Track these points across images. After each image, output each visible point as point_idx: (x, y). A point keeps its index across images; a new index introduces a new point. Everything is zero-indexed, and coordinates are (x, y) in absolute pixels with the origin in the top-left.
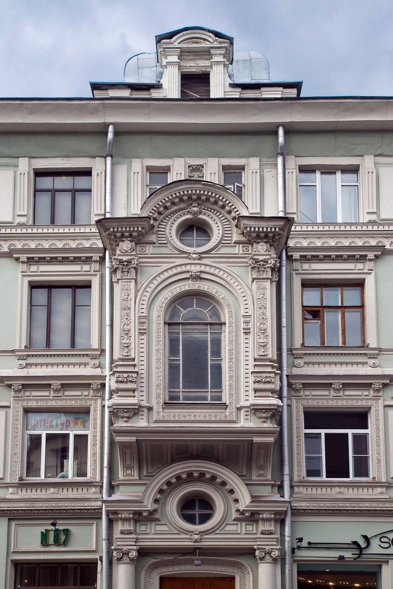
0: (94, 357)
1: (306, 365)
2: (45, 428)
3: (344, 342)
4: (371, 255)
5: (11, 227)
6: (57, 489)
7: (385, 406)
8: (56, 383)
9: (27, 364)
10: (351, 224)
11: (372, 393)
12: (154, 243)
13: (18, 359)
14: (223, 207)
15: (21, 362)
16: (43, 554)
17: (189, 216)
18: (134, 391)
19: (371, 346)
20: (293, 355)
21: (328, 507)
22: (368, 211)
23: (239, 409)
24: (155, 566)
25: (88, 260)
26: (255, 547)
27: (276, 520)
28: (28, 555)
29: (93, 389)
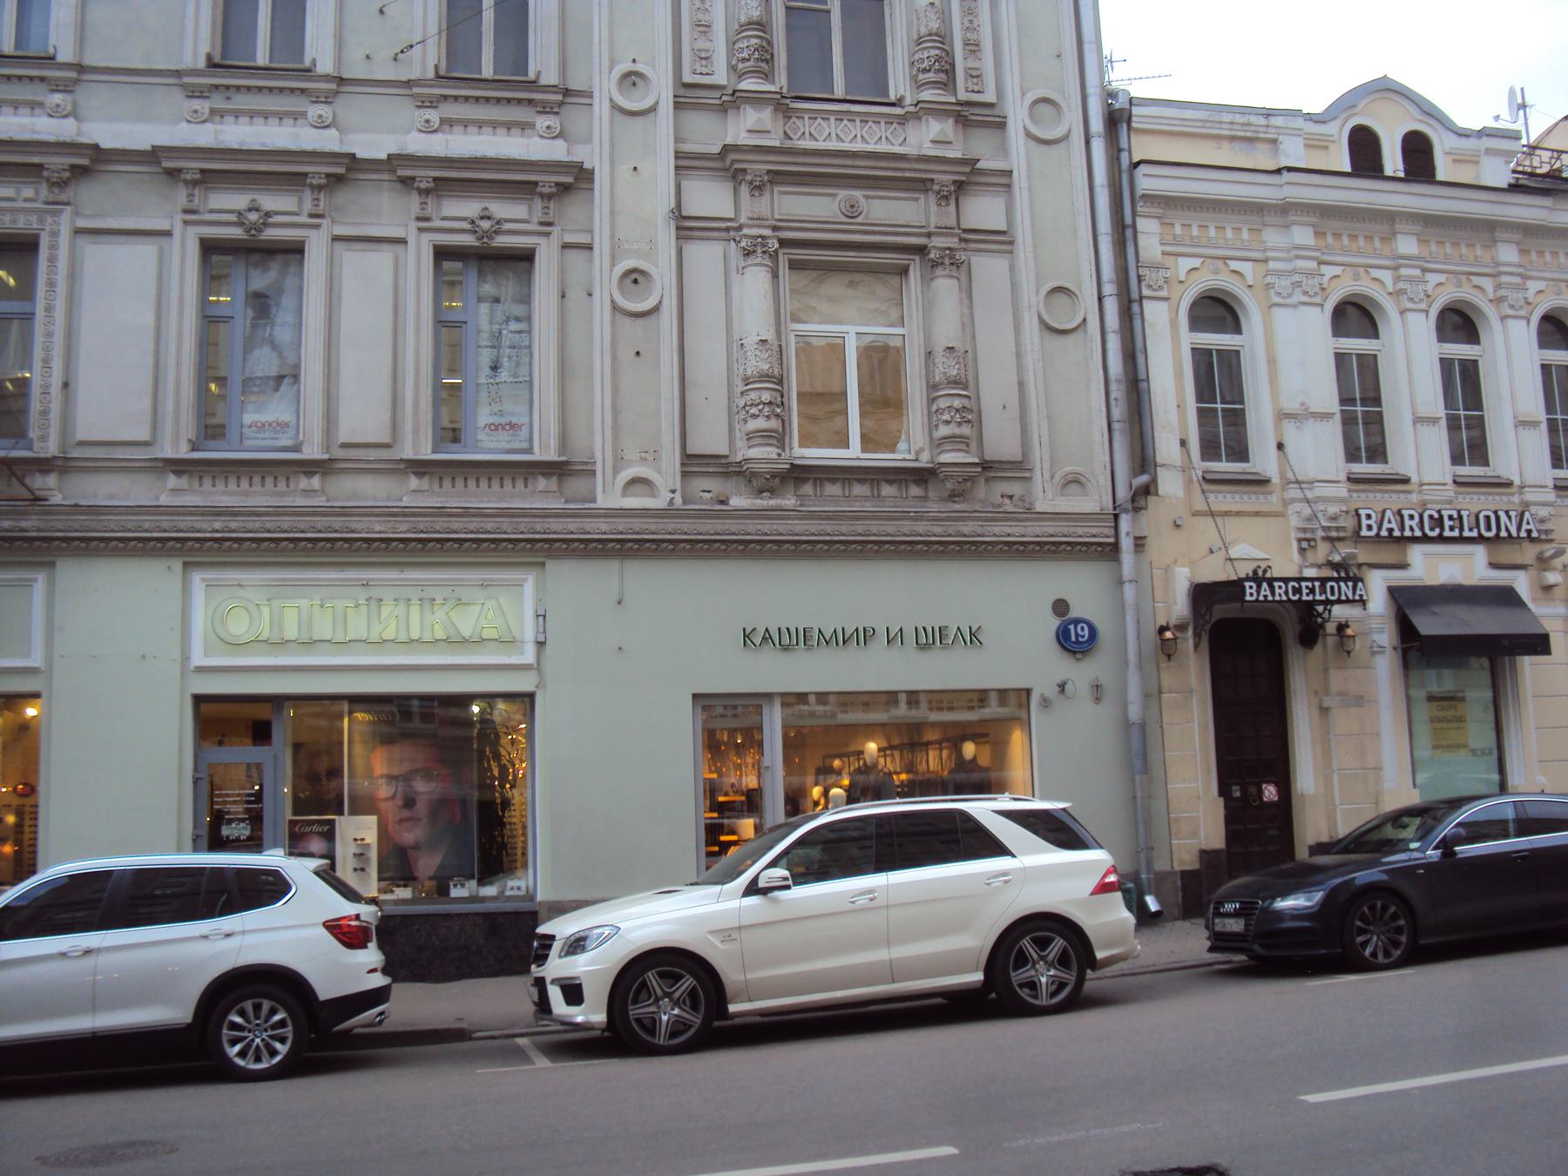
1: (218, 118)
3: (20, 41)
7: (79, 232)
8: (547, 180)
11: (44, 192)
13: (188, 97)
15: (197, 104)
19: (60, 58)
29: (48, 180)
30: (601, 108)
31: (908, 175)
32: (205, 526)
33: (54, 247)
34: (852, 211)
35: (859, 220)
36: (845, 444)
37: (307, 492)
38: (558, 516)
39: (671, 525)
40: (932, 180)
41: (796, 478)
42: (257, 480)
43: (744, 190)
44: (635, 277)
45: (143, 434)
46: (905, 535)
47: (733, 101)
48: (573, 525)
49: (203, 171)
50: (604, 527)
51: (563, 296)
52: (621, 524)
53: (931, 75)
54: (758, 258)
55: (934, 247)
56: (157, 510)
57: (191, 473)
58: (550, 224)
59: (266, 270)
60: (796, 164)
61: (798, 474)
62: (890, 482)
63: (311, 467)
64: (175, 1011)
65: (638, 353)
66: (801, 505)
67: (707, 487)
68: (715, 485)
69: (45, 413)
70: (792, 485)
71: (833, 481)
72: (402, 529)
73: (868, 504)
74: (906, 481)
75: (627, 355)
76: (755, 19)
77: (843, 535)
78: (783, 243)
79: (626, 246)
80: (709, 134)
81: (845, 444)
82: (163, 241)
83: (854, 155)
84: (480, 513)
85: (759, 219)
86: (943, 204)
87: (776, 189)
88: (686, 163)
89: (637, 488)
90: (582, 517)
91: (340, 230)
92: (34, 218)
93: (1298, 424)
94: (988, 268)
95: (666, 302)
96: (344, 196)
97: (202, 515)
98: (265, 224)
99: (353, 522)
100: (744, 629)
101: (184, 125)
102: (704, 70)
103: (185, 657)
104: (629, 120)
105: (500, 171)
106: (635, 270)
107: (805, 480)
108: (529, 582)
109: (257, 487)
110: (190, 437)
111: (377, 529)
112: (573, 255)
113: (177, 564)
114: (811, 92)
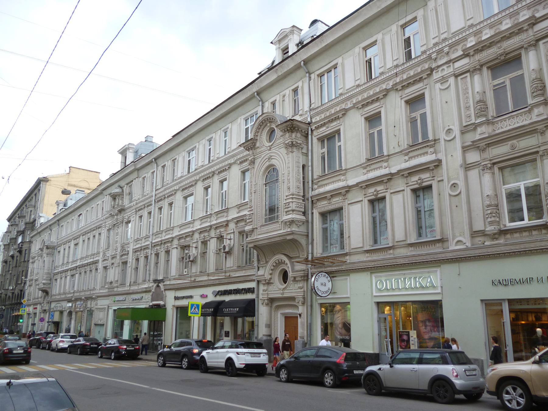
0: (431, 146)
4: (424, 75)
5: (465, 31)
6: (413, 248)
9: (409, 158)
10: (504, 10)
12: (259, 147)
17: (268, 129)
18: (252, 221)
22: (433, 38)
24: (278, 307)
26: (295, 297)
27: (304, 280)
30: (442, 142)
31: (528, 130)
32: (370, 264)
33: (345, 208)
36: (523, 220)
37: (390, 254)
38: (439, 253)
39: (468, 252)
41: (504, 233)
42: (381, 252)
44: (454, 185)
45: (361, 245)
46: (538, 247)
47: (475, 126)
48: (443, 255)
49: (366, 185)
50: (451, 255)
51: (440, 195)
52: (455, 254)
53: (535, 93)
54: (486, 171)
55: (541, 151)
56: (362, 262)
57: (370, 253)
58: (434, 177)
59: (382, 203)
60: (493, 140)
61: (504, 232)
62: (535, 230)
63: (390, 248)
65: (457, 206)
66: (506, 241)
67: (479, 240)
68: (482, 239)
69: (346, 243)
70: (503, 236)
71: (516, 232)
72: (406, 261)
73: (527, 238)
74: (541, 229)
75: (454, 207)
76: (478, 100)
77: (517, 249)
78: (494, 164)
79: (452, 177)
80: (471, 137)
81: (523, 220)
82: (361, 202)
83: (509, 131)
84: (422, 255)
85: (484, 159)
86: (543, 135)
87: (490, 148)
88: (465, 149)
89: (459, 243)
90: (445, 253)
91: (392, 191)
92: (342, 203)
93: (266, 301)
95: (462, 190)
96: (392, 182)
97: (370, 262)
98: (378, 194)
99: (398, 260)
100: (492, 280)
101: (362, 176)
103: (372, 293)
104: (450, 143)
105: (420, 167)
106: (454, 184)
107: (507, 233)
108: (438, 270)
109: (375, 255)
111: (402, 261)
112: (441, 183)
113: (369, 273)
114: (502, 113)
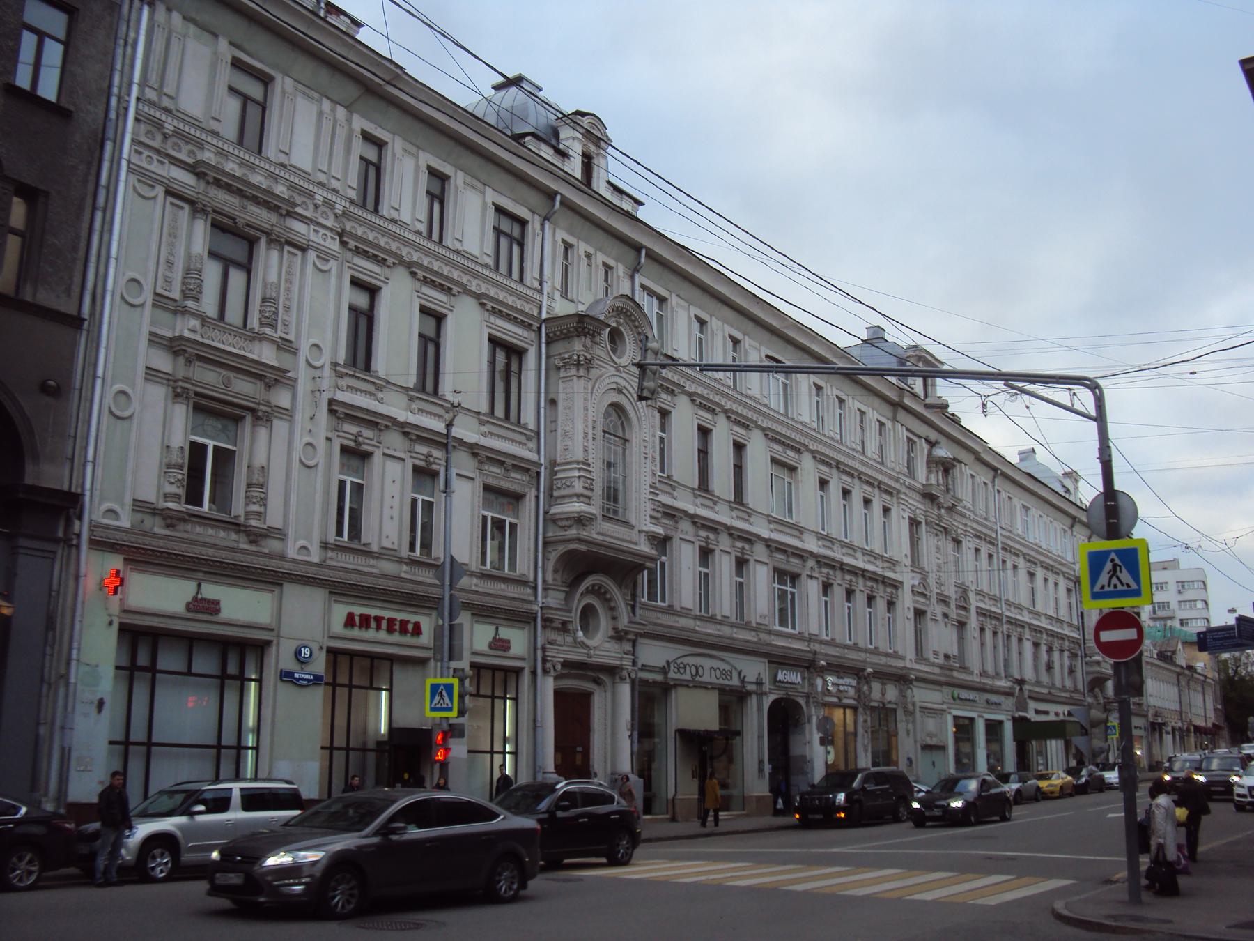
2: (213, 439)
14: (637, 327)
16: (408, 649)
20: (336, 371)
21: (102, 537)
23: (640, 532)
25: (528, 327)
28: (373, 645)
34: (227, 383)
35: (230, 389)
40: (265, 376)
43: (181, 360)
64: (925, 656)
94: (280, 426)
102: (168, 288)
110: (610, 635)
